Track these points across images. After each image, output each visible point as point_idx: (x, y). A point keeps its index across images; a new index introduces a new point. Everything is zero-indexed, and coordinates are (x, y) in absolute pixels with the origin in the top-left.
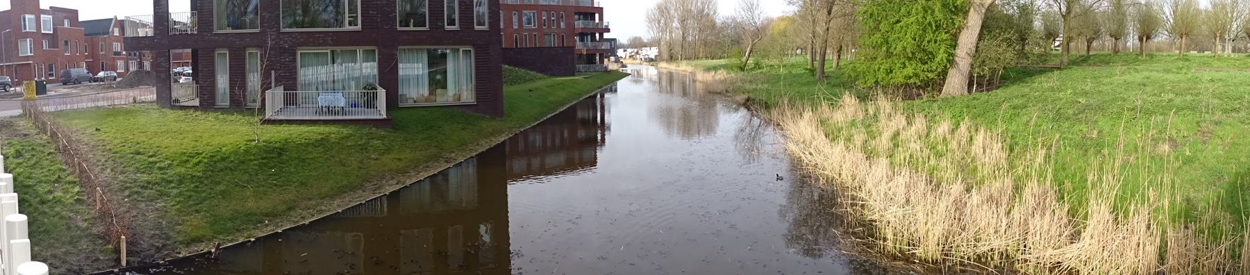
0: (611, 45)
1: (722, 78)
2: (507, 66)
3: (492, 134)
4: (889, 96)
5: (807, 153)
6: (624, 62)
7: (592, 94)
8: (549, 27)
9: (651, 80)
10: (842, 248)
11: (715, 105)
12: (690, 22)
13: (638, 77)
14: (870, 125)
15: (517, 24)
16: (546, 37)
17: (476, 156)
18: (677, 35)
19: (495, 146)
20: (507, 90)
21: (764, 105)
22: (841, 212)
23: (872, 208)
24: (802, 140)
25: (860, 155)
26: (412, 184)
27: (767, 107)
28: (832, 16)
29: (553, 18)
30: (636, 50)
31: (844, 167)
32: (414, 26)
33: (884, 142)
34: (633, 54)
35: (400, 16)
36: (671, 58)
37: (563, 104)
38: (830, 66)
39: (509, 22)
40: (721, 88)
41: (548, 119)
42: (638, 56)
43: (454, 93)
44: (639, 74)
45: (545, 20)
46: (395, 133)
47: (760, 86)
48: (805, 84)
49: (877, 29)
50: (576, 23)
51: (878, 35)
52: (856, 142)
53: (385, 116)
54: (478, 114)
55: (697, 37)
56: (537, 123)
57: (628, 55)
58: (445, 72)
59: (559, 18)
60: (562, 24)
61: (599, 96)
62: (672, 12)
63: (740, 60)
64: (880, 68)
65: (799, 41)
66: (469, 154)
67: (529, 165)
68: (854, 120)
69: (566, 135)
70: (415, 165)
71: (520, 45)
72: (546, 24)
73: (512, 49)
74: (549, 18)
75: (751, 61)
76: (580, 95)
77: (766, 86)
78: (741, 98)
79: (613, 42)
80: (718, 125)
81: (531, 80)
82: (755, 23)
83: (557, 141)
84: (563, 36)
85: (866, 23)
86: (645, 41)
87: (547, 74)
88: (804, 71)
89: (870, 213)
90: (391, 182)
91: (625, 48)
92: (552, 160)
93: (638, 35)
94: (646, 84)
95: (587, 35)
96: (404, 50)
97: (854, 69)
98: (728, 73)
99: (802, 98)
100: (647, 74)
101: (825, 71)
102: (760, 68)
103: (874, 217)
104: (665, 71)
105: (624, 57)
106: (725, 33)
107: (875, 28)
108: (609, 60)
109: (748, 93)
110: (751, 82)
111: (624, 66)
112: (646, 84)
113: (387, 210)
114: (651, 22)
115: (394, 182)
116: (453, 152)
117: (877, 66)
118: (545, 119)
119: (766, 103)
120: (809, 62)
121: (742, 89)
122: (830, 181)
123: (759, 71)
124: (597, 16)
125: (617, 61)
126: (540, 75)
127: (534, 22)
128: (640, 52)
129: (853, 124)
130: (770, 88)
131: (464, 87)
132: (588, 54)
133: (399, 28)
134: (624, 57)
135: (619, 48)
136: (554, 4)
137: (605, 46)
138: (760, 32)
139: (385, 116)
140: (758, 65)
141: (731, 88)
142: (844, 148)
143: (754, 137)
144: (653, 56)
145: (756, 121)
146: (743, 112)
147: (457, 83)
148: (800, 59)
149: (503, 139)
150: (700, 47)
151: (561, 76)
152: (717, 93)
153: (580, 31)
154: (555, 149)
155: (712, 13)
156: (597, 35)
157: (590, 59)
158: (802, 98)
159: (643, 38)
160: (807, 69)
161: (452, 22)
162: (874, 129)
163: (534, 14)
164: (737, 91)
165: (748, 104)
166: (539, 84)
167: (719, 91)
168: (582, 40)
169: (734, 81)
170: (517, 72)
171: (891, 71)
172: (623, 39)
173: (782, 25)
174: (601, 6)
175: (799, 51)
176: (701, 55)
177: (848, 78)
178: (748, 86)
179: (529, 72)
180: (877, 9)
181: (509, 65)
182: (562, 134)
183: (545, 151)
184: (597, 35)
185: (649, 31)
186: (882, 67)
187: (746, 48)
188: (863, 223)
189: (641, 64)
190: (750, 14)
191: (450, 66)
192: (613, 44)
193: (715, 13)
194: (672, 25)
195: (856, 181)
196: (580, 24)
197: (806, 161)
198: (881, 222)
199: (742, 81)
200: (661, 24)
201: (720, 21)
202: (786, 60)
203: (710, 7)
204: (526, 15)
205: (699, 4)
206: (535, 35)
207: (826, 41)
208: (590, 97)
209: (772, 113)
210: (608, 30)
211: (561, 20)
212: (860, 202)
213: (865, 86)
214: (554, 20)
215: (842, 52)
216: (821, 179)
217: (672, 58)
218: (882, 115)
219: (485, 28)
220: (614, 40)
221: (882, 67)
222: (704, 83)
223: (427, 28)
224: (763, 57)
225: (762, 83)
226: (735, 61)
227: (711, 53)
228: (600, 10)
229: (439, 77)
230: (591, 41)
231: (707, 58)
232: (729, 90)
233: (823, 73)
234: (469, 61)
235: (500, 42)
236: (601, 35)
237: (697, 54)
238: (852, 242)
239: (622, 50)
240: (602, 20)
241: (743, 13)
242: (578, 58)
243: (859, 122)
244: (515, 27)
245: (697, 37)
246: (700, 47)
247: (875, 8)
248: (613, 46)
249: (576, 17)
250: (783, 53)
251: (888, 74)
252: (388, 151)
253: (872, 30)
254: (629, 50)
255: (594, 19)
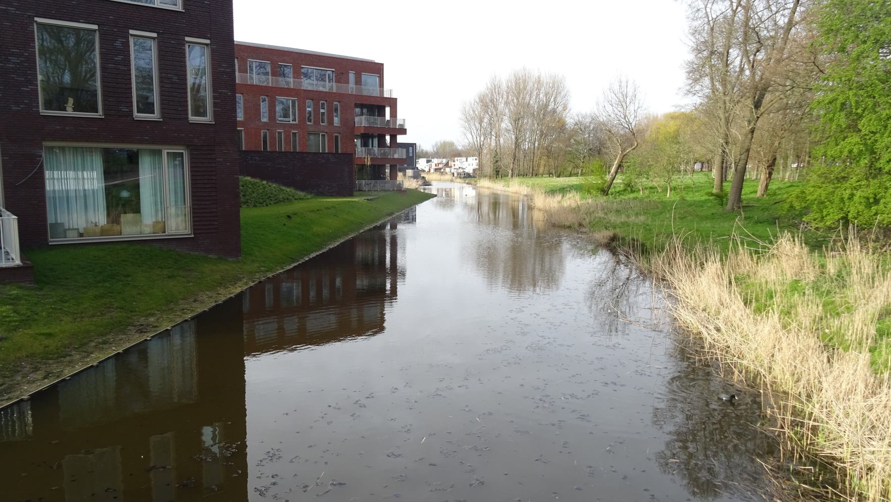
0: (408, 152)
1: (574, 205)
2: (249, 178)
3: (220, 284)
4: (871, 245)
5: (711, 327)
6: (428, 177)
7: (378, 224)
8: (316, 123)
9: (466, 205)
10: (775, 494)
11: (558, 244)
12: (527, 122)
13: (448, 202)
14: (829, 292)
15: (266, 115)
16: (312, 137)
17: (192, 318)
18: (507, 140)
19: (225, 302)
20: (247, 214)
21: (640, 248)
22: (773, 432)
23: (832, 436)
24: (702, 306)
25: (812, 341)
26: (102, 361)
27: (645, 251)
28: (762, 109)
29: (322, 111)
30: (444, 161)
31: (778, 357)
32: (74, 110)
33: (858, 324)
34: (440, 166)
35: (44, 89)
36: (497, 173)
37: (334, 238)
38: (752, 189)
39: (253, 112)
40: (571, 219)
41: (310, 260)
42: (448, 170)
43: (154, 220)
44: (448, 194)
45: (310, 113)
46: (41, 289)
47: (633, 218)
48: (706, 218)
49: (853, 127)
50: (357, 119)
51: (854, 139)
52: (801, 317)
53: (18, 262)
54: (196, 253)
55: (536, 145)
56: (293, 265)
57: (434, 167)
58: (135, 188)
59: (332, 111)
60: (336, 120)
61: (388, 227)
62: (501, 106)
63: (602, 178)
64: (852, 195)
65: (699, 151)
66: (180, 316)
67: (281, 329)
68: (797, 281)
69: (338, 282)
70: (82, 344)
71: (271, 147)
72: (312, 118)
73: (258, 152)
74: (316, 110)
75: (619, 180)
76: (361, 225)
77: (642, 218)
78: (602, 235)
79: (411, 148)
80: (563, 273)
81: (287, 200)
82: (629, 123)
83: (326, 292)
84: (337, 137)
85: (831, 120)
86: (460, 148)
87: (311, 193)
88: (707, 197)
89: (827, 443)
90: (32, 376)
91: (428, 157)
92: (316, 322)
93: (448, 139)
94: (458, 210)
95: (373, 137)
96: (52, 148)
97: (802, 196)
98: (582, 198)
99: (705, 238)
100: (461, 196)
101: (743, 197)
102: (633, 192)
103: (837, 453)
104: (486, 192)
105: (427, 170)
106: (579, 138)
107: (849, 127)
108: (405, 175)
109: (614, 228)
110: (618, 211)
111: (427, 183)
112: (458, 210)
113: (33, 421)
114: (469, 121)
115: (39, 375)
116: (152, 315)
117: (848, 192)
118: (307, 259)
119: (643, 245)
120: (716, 182)
121: (604, 221)
122: (753, 380)
123: (632, 196)
124: (388, 110)
125: (417, 175)
126: (301, 194)
127: (294, 115)
128: (451, 163)
129: (795, 286)
130: (649, 222)
131: (172, 210)
132: (374, 165)
133: (43, 112)
134: (427, 170)
135: (420, 157)
136: (324, 90)
137: (399, 154)
138: (632, 137)
139: (18, 262)
140: (629, 187)
141: (587, 220)
142: (779, 326)
143: (619, 295)
144: (469, 170)
145: (623, 272)
146: (604, 256)
147: (160, 204)
148: (700, 178)
149: (238, 290)
150: (540, 159)
151: (332, 195)
152: (565, 227)
153: (363, 132)
154: (320, 304)
155: (560, 108)
156: (388, 138)
157: (376, 171)
158: (705, 238)
159: (456, 143)
160: (712, 195)
161: (147, 107)
162: (837, 299)
163: (294, 102)
164: (595, 225)
165: (614, 244)
166: (297, 207)
167: (568, 224)
168: (365, 144)
169: (591, 210)
170: (264, 188)
171: (877, 201)
172: (425, 144)
173: (672, 126)
174: (394, 96)
175: (697, 166)
176: (541, 170)
177: (788, 211)
178: (613, 218)
179: (284, 188)
180: (855, 95)
181: (253, 176)
182: (333, 283)
183: (305, 307)
184: (388, 138)
185: (465, 135)
186: (858, 193)
187: (612, 161)
188: (814, 459)
189: (452, 181)
190: (620, 109)
191: (146, 176)
192: (411, 150)
193: (565, 108)
194: (499, 126)
195: (801, 384)
196: (362, 121)
197: (709, 339)
198: (852, 464)
199: (606, 210)
200: (484, 125)
201: (572, 121)
202: (678, 180)
203: (559, 99)
204: (282, 103)
205: (541, 96)
206: (294, 134)
207: (748, 150)
208: (375, 228)
209: (653, 261)
210: (403, 131)
211: (335, 114)
212: (811, 423)
213: (821, 225)
214: (323, 113)
215: (775, 168)
216: (736, 372)
217: (498, 174)
218: (855, 277)
219: (208, 119)
220: (413, 145)
221: (858, 193)
222: (548, 213)
223: (100, 114)
224: (640, 174)
225: (637, 215)
226: (594, 180)
227: (556, 167)
228: (393, 103)
229: (125, 194)
230: (379, 147)
231: (550, 174)
232: (584, 223)
233: (739, 199)
234: (179, 170)
235: (239, 145)
236: (393, 138)
237: (535, 168)
238: (796, 489)
239: (425, 160)
240: (396, 116)
241: (609, 108)
242: (359, 170)
243: (807, 284)
244: (265, 119)
245: (536, 145)
246: (540, 159)
247: (851, 93)
248: (411, 153)
249: (358, 110)
250: (673, 169)
251: (869, 206)
252: (26, 322)
253: (842, 131)
254: (435, 161)
255: (384, 115)
